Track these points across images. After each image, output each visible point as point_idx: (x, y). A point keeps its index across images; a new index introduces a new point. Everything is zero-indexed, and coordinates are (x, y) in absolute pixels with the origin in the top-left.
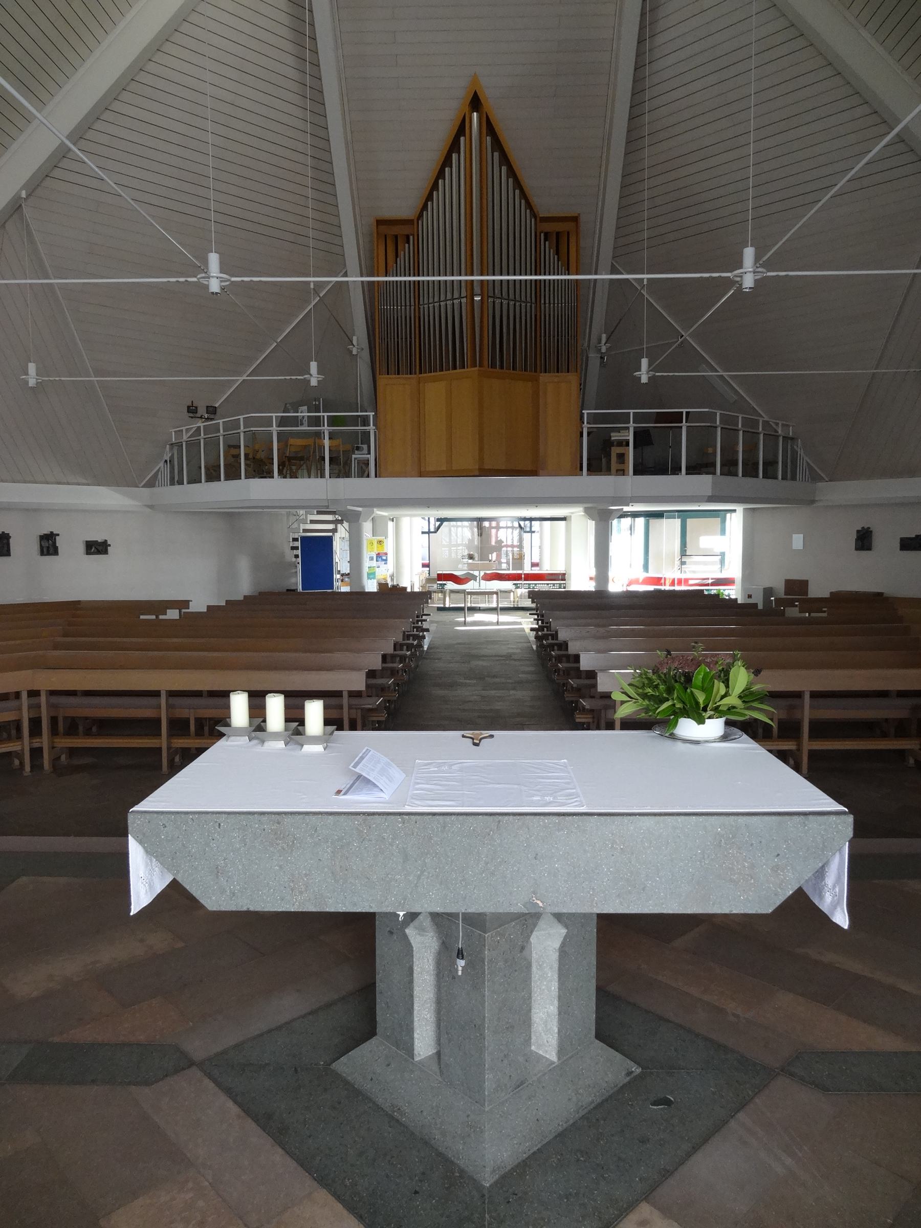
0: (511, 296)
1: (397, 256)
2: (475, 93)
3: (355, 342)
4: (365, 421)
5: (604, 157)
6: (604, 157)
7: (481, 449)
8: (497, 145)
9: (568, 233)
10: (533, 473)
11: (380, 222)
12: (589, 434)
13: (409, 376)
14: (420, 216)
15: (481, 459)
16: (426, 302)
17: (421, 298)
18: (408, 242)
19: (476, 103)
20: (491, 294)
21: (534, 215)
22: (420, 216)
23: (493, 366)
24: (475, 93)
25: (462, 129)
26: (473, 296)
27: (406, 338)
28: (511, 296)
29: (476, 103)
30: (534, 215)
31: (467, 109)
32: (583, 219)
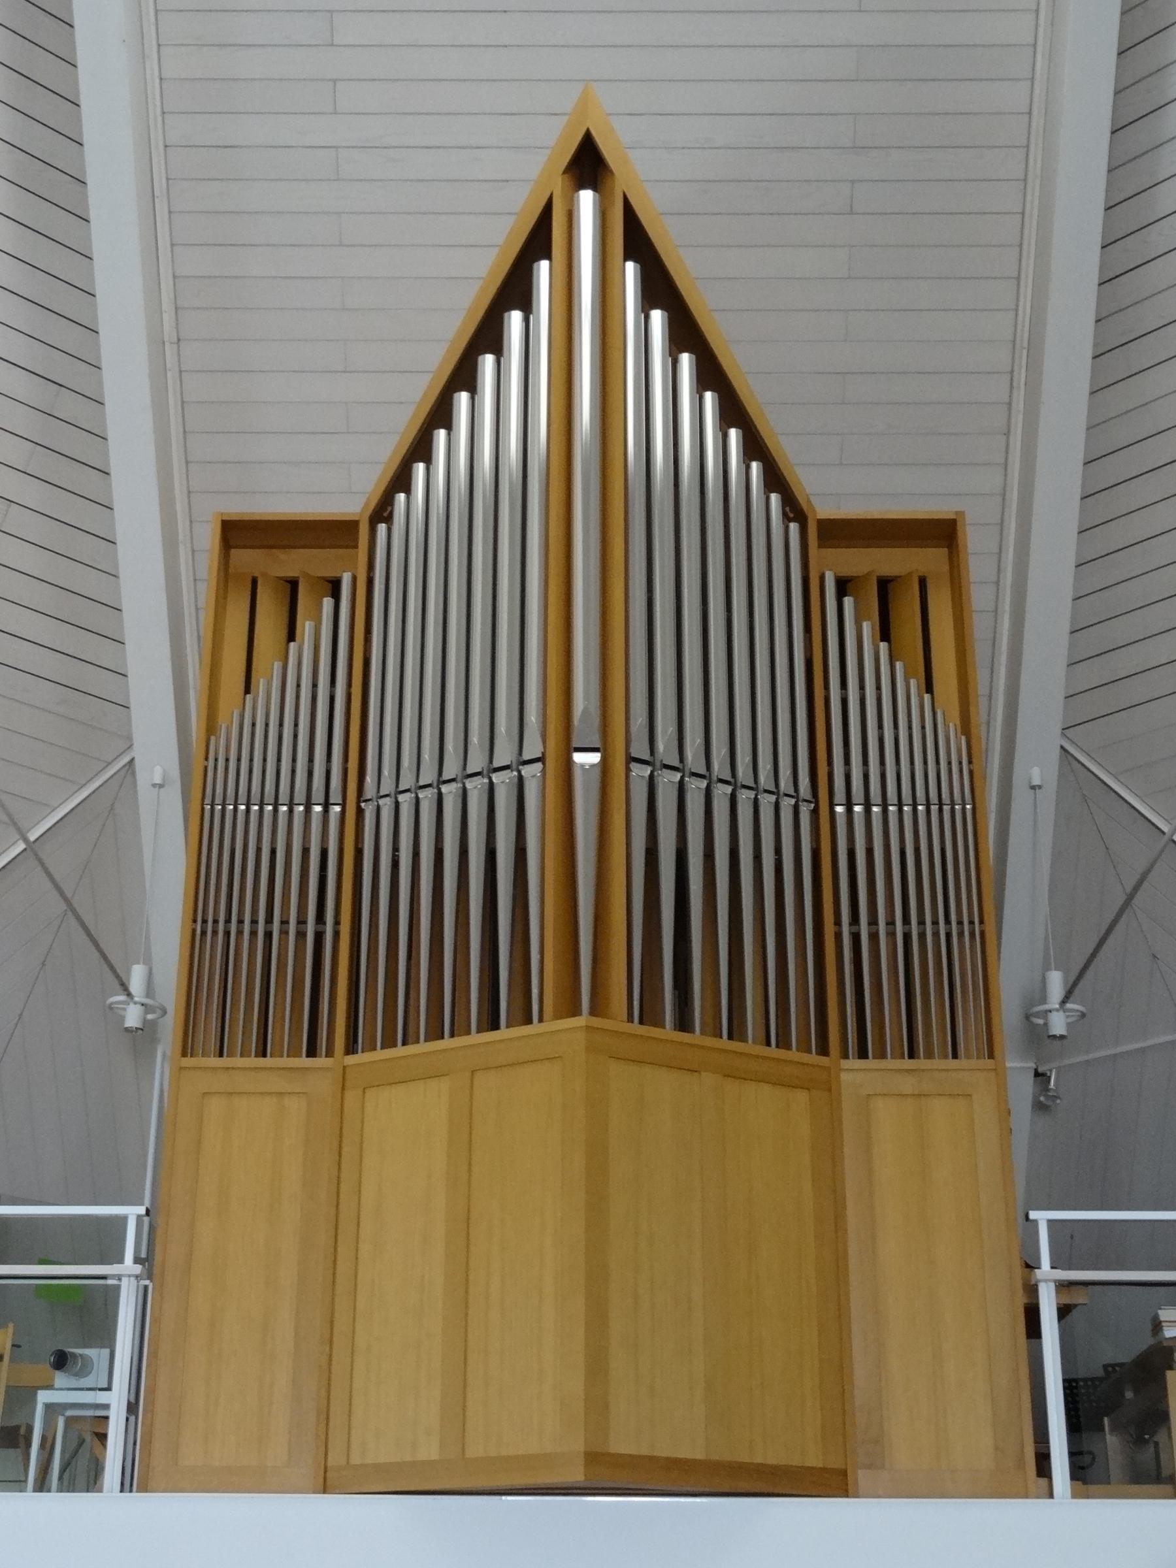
0: (719, 766)
1: (291, 636)
2: (588, 130)
3: (137, 983)
4: (102, 1240)
5: (1019, 405)
6: (1019, 405)
7: (597, 1367)
8: (660, 288)
9: (923, 582)
10: (831, 1482)
11: (236, 533)
12: (1064, 1312)
13: (304, 1061)
14: (382, 512)
15: (597, 1407)
16: (387, 786)
17: (369, 779)
18: (336, 595)
19: (588, 165)
20: (640, 749)
21: (794, 510)
22: (382, 512)
23: (649, 1015)
24: (588, 130)
25: (539, 241)
26: (569, 748)
27: (301, 922)
28: (719, 766)
29: (588, 165)
30: (794, 510)
31: (558, 185)
32: (974, 540)
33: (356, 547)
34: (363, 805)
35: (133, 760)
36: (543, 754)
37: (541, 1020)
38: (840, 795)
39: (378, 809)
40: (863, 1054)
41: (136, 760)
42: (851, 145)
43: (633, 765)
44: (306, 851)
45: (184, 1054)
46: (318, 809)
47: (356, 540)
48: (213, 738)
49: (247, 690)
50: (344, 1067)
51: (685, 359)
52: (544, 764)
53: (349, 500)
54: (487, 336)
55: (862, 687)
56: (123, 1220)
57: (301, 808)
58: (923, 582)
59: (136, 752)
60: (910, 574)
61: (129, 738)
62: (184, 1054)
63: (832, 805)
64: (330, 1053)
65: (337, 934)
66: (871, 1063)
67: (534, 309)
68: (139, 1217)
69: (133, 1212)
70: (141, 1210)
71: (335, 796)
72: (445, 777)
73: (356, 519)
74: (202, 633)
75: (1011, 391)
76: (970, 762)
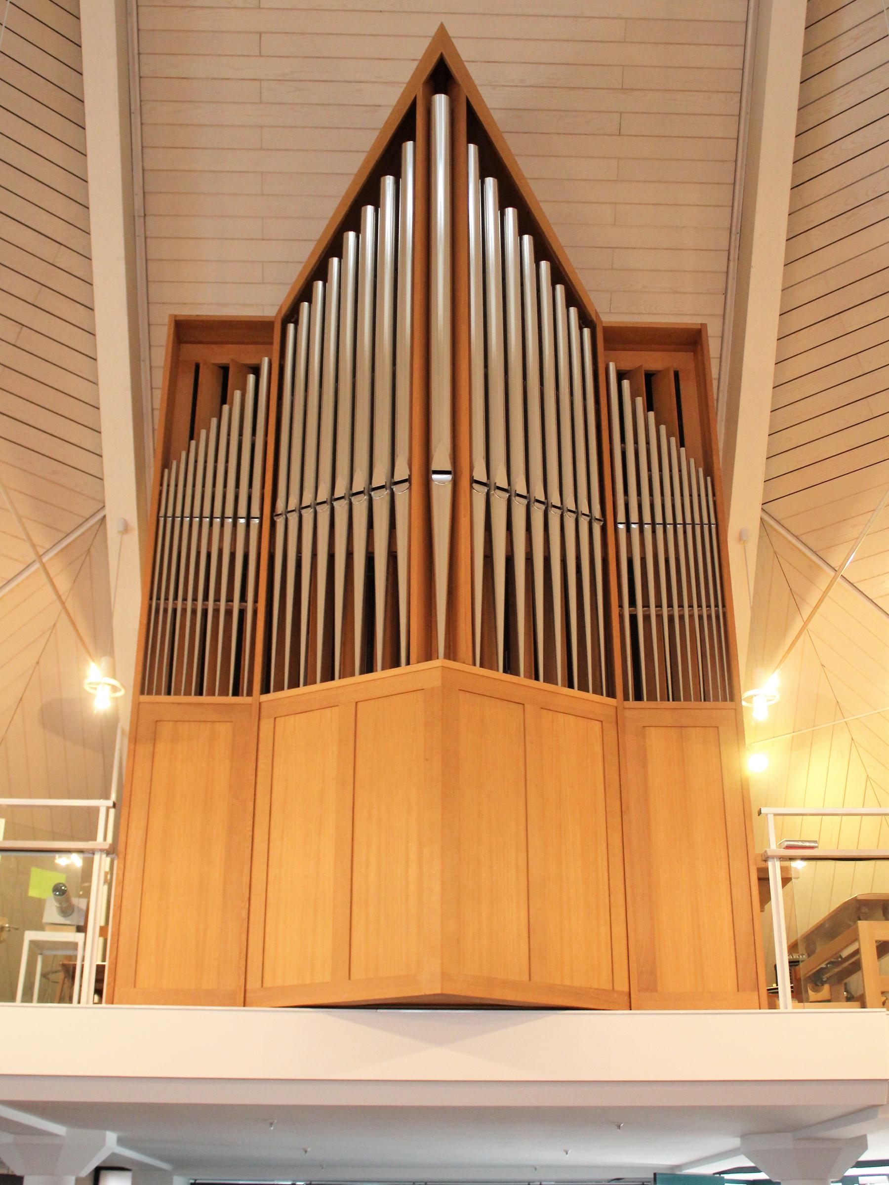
9: (676, 374)
13: (230, 699)
14: (292, 315)
19: (441, 76)
21: (585, 320)
22: (292, 315)
23: (487, 662)
29: (441, 76)
30: (585, 320)
33: (272, 343)
34: (275, 518)
35: (104, 517)
36: (410, 476)
37: (408, 663)
38: (621, 517)
39: (287, 520)
40: (638, 697)
41: (107, 517)
42: (620, 87)
43: (475, 485)
44: (233, 555)
45: (142, 693)
46: (242, 521)
47: (272, 338)
48: (166, 471)
49: (191, 438)
50: (260, 703)
51: (510, 212)
52: (410, 483)
53: (267, 303)
54: (369, 193)
55: (636, 442)
56: (97, 810)
57: (230, 520)
58: (676, 374)
59: (107, 512)
60: (667, 370)
61: (104, 502)
62: (142, 693)
63: (616, 524)
64: (250, 693)
65: (255, 612)
66: (645, 703)
67: (403, 175)
68: (108, 809)
69: (103, 804)
70: (110, 803)
71: (255, 512)
72: (337, 495)
73: (273, 319)
74: (156, 427)
75: (728, 263)
76: (714, 495)
